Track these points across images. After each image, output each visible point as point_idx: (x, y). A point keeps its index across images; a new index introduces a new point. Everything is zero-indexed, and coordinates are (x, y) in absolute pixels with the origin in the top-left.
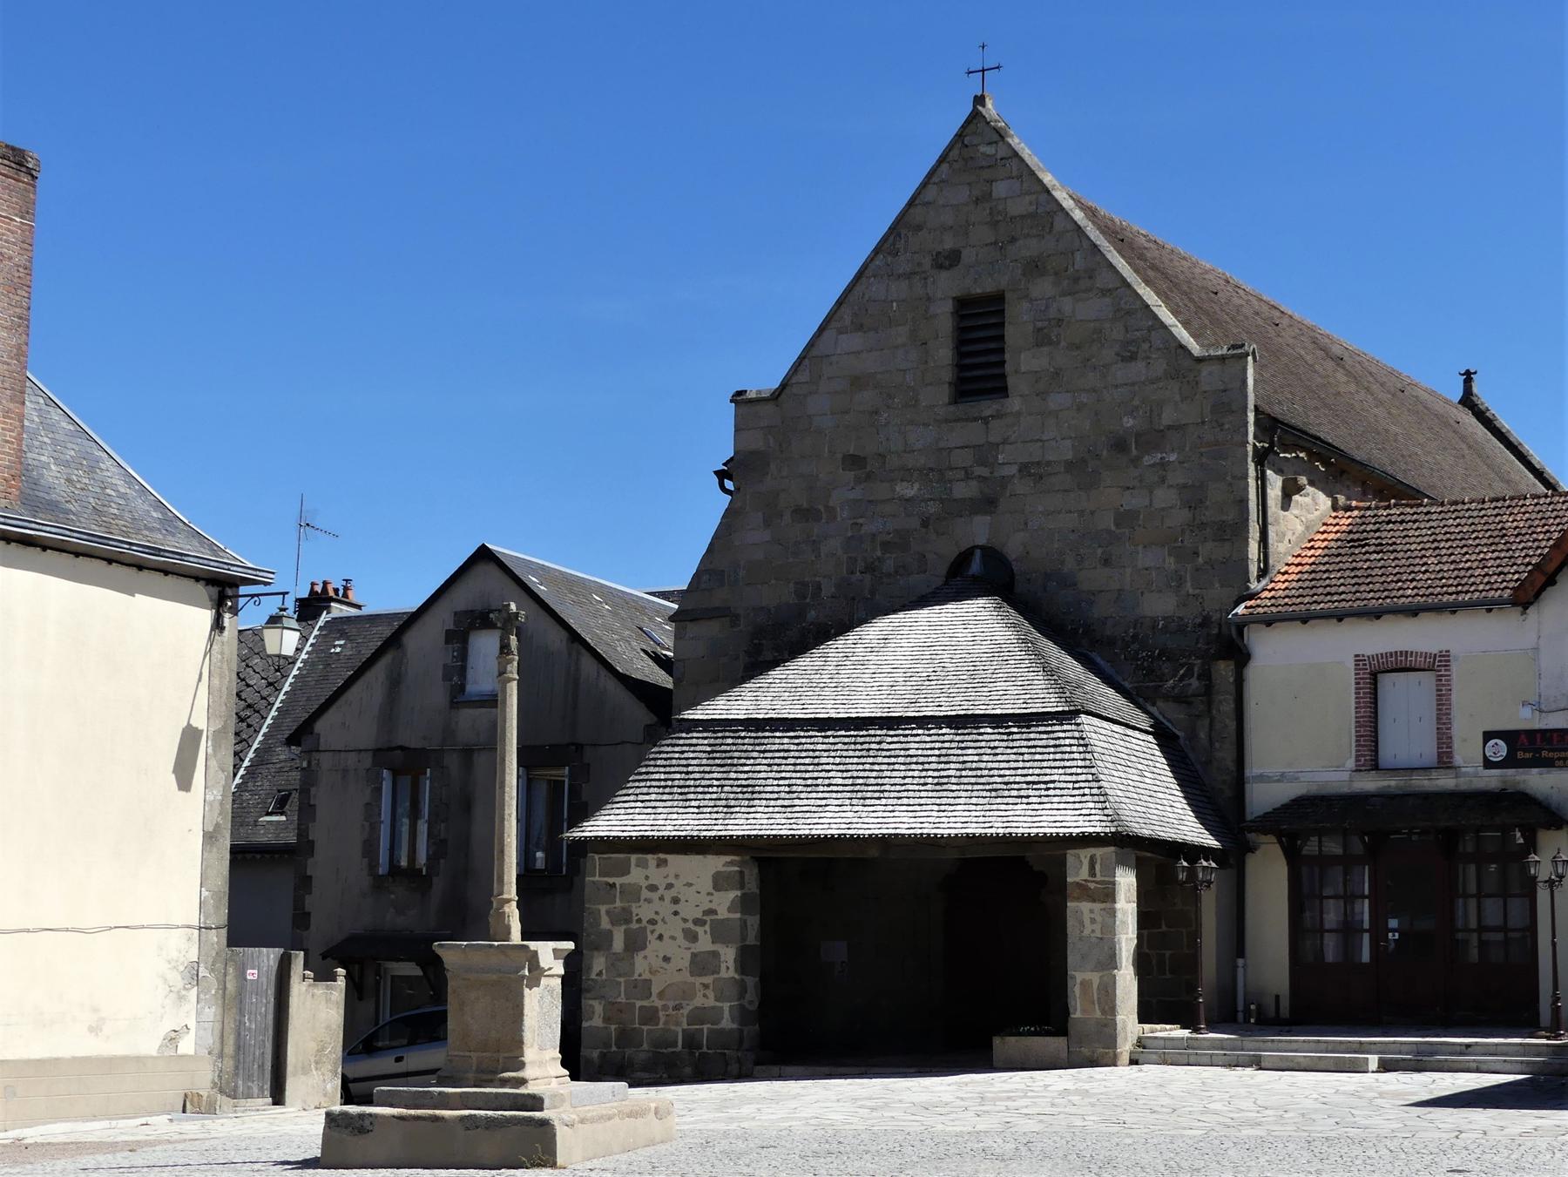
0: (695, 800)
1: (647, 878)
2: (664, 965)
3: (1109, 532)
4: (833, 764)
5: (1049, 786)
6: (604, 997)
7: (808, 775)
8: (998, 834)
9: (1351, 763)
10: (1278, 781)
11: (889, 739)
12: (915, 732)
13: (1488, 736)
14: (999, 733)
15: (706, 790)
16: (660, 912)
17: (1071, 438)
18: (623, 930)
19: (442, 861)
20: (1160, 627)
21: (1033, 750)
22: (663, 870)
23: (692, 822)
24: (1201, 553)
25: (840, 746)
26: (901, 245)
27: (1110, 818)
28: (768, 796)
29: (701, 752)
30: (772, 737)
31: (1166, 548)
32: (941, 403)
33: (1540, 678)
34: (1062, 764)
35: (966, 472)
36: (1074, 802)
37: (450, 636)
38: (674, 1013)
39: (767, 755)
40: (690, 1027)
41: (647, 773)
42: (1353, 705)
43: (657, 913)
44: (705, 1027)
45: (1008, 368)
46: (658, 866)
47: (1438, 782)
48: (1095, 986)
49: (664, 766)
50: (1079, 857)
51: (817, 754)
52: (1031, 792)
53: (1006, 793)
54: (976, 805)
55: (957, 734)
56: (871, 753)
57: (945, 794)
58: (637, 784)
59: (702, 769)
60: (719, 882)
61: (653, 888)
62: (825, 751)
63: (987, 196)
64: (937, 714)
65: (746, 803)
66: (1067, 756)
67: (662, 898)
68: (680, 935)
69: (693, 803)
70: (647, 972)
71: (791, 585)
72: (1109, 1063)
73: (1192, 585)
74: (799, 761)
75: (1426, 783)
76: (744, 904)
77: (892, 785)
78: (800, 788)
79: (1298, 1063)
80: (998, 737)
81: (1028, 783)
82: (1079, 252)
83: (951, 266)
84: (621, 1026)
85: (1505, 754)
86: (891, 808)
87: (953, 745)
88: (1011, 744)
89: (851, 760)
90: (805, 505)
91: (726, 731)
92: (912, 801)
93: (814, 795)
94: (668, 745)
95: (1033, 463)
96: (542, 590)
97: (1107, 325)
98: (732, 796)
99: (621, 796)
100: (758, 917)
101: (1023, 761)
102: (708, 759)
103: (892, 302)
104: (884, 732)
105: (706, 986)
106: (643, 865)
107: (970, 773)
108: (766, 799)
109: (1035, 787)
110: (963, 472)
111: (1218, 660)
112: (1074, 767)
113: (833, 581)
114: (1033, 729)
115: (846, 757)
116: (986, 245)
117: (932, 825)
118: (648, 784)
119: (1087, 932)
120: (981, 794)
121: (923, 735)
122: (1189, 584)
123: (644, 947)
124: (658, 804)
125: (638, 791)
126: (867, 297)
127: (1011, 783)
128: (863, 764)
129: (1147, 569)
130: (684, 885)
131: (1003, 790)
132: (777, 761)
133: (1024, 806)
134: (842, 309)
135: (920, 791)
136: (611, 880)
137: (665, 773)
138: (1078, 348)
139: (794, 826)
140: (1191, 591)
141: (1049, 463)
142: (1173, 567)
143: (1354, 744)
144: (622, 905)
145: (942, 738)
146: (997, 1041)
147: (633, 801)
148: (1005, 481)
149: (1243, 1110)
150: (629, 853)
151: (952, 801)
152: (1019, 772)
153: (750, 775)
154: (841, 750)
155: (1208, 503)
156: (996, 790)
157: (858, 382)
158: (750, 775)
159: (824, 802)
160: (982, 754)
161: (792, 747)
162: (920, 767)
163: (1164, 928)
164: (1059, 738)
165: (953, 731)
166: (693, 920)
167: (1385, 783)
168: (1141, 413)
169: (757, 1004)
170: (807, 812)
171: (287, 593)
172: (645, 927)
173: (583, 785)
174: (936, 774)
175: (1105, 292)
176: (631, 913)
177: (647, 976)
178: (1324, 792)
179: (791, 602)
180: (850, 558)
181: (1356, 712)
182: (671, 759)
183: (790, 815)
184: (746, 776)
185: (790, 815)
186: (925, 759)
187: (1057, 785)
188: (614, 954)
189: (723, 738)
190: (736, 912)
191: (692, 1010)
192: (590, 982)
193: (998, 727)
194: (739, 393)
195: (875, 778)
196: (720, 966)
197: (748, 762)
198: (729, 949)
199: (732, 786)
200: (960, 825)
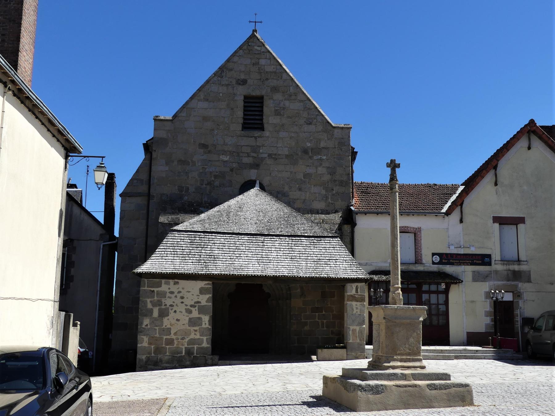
1: (169, 289)
2: (177, 322)
3: (301, 180)
6: (148, 335)
10: (365, 265)
13: (433, 254)
16: (175, 302)
17: (288, 147)
18: (158, 309)
22: (177, 286)
24: (334, 190)
26: (224, 74)
31: (322, 186)
33: (449, 238)
35: (248, 155)
38: (181, 341)
40: (188, 346)
43: (174, 302)
44: (195, 346)
45: (264, 121)
46: (174, 284)
47: (417, 268)
48: (357, 331)
50: (352, 287)
60: (202, 291)
61: (172, 293)
63: (258, 63)
67: (176, 297)
68: (184, 311)
71: (177, 187)
73: (331, 200)
75: (414, 268)
82: (292, 87)
83: (243, 84)
84: (156, 346)
85: (439, 260)
90: (183, 159)
95: (273, 154)
97: (301, 112)
103: (220, 93)
105: (196, 331)
106: (168, 284)
113: (194, 187)
116: (257, 79)
119: (354, 312)
122: (330, 200)
126: (210, 90)
129: (315, 193)
136: (152, 289)
138: (291, 118)
141: (279, 155)
142: (324, 193)
144: (158, 299)
148: (263, 159)
150: (161, 279)
155: (337, 174)
157: (205, 119)
163: (324, 313)
166: (190, 305)
168: (313, 142)
171: (104, 157)
172: (168, 308)
173: (73, 255)
175: (301, 101)
176: (162, 302)
177: (169, 326)
178: (381, 269)
179: (176, 193)
188: (154, 318)
190: (210, 303)
191: (189, 340)
194: (157, 116)
198: (206, 317)
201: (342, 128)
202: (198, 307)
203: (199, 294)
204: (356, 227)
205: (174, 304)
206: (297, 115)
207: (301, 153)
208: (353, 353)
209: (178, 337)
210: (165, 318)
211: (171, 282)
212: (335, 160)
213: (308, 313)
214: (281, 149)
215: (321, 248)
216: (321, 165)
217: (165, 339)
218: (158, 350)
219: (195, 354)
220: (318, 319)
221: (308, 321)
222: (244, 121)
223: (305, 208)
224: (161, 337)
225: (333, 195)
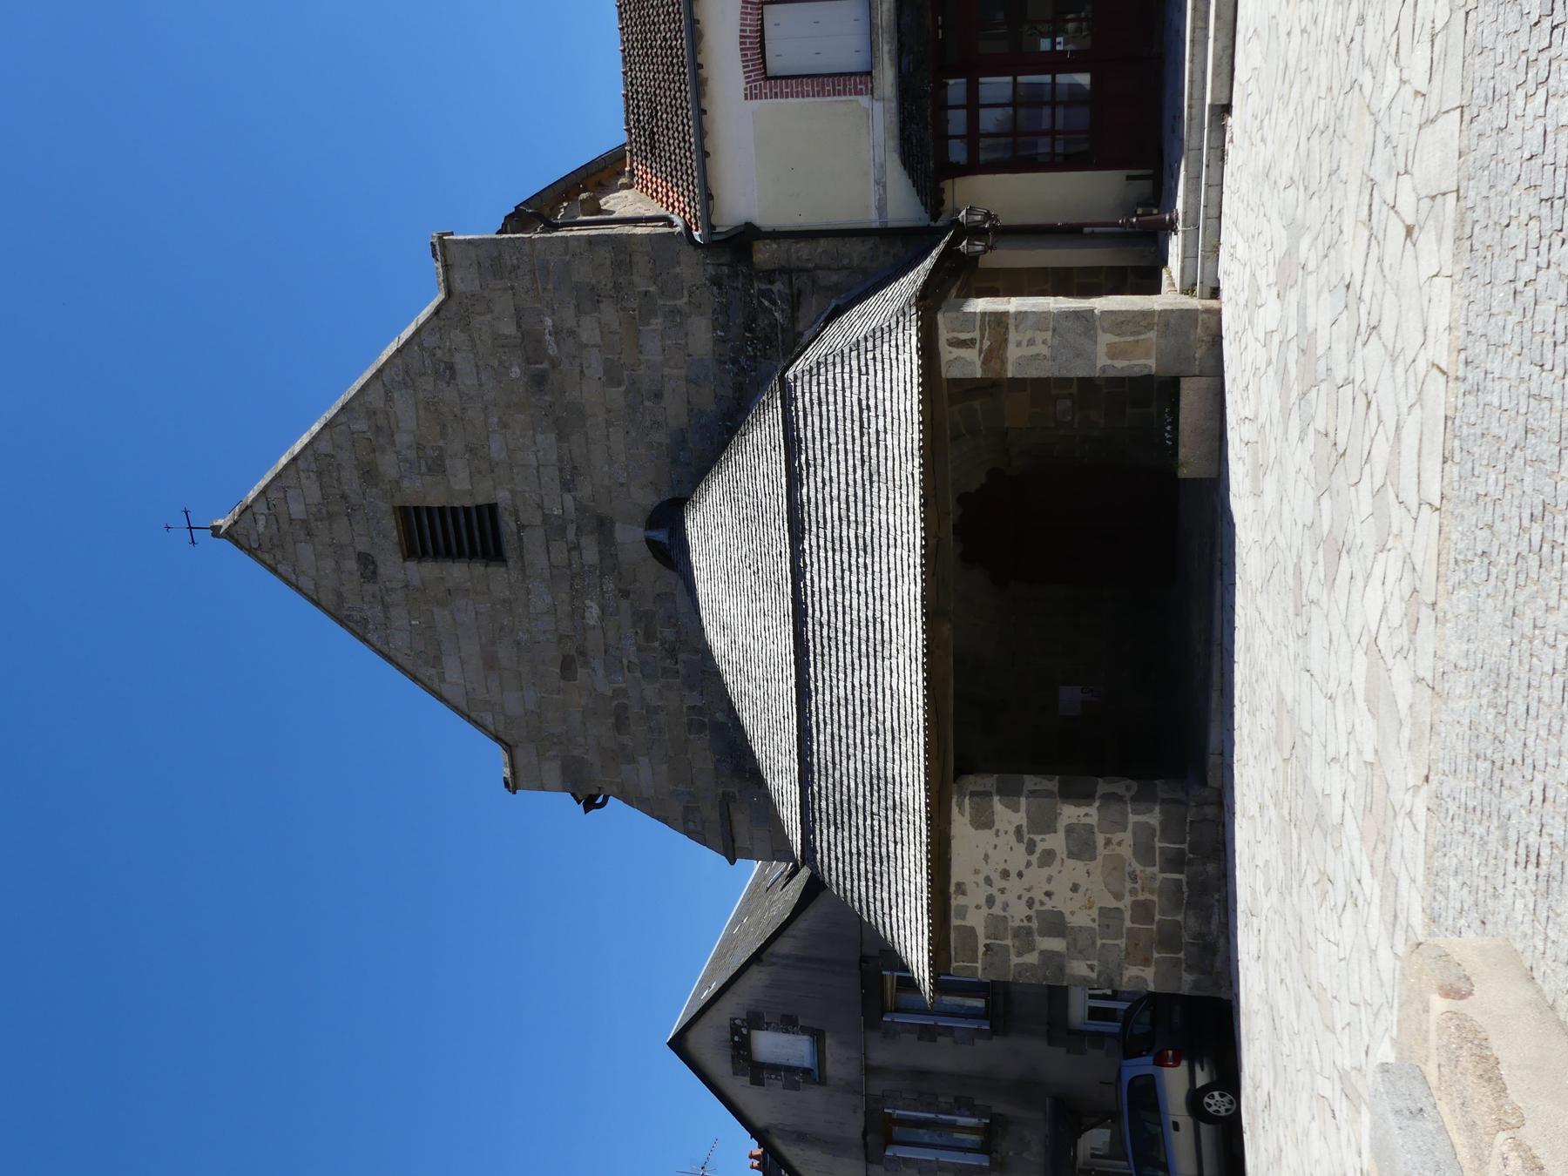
0: (888, 846)
1: (978, 907)
2: (1082, 890)
3: (627, 393)
4: (845, 681)
5: (864, 407)
6: (1119, 965)
7: (858, 712)
8: (920, 465)
9: (864, 100)
10: (884, 187)
11: (817, 613)
12: (809, 583)
14: (808, 477)
15: (876, 833)
17: (534, 436)
19: (976, 1102)
20: (722, 334)
21: (825, 432)
22: (970, 887)
23: (912, 852)
24: (644, 289)
25: (826, 674)
27: (901, 319)
28: (882, 760)
29: (836, 838)
30: (818, 754)
32: (506, 576)
34: (839, 393)
35: (573, 549)
36: (883, 370)
37: (757, 1081)
38: (1139, 881)
39: (837, 761)
41: (860, 901)
42: (800, 100)
43: (1020, 897)
44: (1158, 845)
45: (468, 503)
46: (964, 893)
48: (1115, 339)
49: (852, 880)
51: (835, 701)
52: (873, 430)
53: (874, 461)
54: (888, 499)
55: (810, 531)
56: (833, 635)
57: (876, 540)
58: (872, 913)
59: (854, 837)
60: (983, 821)
61: (990, 901)
62: (831, 691)
64: (788, 556)
65: (890, 786)
66: (831, 388)
67: (1002, 891)
68: (1046, 871)
69: (891, 849)
70: (1091, 912)
71: (692, 737)
72: (1215, 318)
74: (843, 722)
76: (1009, 793)
77: (867, 608)
78: (873, 721)
79: (1223, 51)
80: (812, 479)
81: (862, 435)
83: (373, 562)
86: (893, 608)
87: (822, 534)
88: (819, 461)
89: (841, 659)
90: (613, 720)
91: (813, 808)
92: (885, 582)
93: (880, 704)
94: (830, 875)
96: (714, 986)
97: (421, 395)
98: (883, 803)
99: (885, 932)
100: (1025, 776)
101: (837, 443)
102: (843, 830)
103: (411, 625)
104: (809, 620)
105: (1108, 842)
107: (852, 510)
108: (886, 761)
109: (866, 425)
110: (573, 553)
111: (752, 262)
112: (843, 377)
114: (802, 435)
115: (838, 666)
117: (912, 554)
118: (871, 900)
119: (1044, 350)
120: (875, 495)
121: (811, 572)
123: (1061, 914)
124: (893, 890)
125: (879, 912)
126: (408, 652)
127: (862, 456)
128: (845, 644)
130: (987, 863)
131: (870, 466)
132: (844, 749)
133: (889, 436)
134: (421, 676)
135: (873, 572)
136: (981, 949)
137: (859, 880)
138: (444, 426)
139: (915, 727)
140: (685, 300)
141: (560, 459)
142: (660, 320)
143: (843, 98)
144: (1010, 937)
145: (815, 549)
146: (1184, 473)
147: (891, 918)
148: (581, 508)
149: (1291, 87)
150: (949, 927)
151: (884, 531)
152: (849, 447)
153: (859, 780)
154: (830, 671)
155: (594, 281)
156: (871, 475)
157: (490, 662)
158: (859, 780)
159: (888, 692)
160: (831, 497)
161: (829, 730)
162: (847, 573)
164: (811, 400)
165: (807, 536)
167: (886, 57)
169: (1129, 782)
170: (899, 712)
172: (1038, 912)
174: (854, 554)
175: (388, 398)
176: (1020, 927)
177: (1095, 913)
180: (662, 675)
181: (808, 96)
182: (844, 872)
183: (903, 734)
184: (861, 786)
185: (903, 734)
186: (838, 568)
187: (863, 396)
188: (1068, 949)
189: (820, 812)
190: (1019, 801)
192: (1101, 980)
193: (801, 480)
194: (507, 784)
195: (860, 629)
196: (1084, 825)
197: (845, 783)
199: (872, 803)
200: (911, 516)
201: (447, 267)
202: (1034, 834)
203: (994, 829)
204: (758, 222)
205: (1026, 896)
206: (432, 408)
207: (546, 394)
208: (1197, 356)
209: (1127, 890)
210: (1067, 920)
211: (956, 901)
212: (550, 286)
214: (541, 453)
215: (825, 445)
216: (572, 333)
217: (1133, 923)
218: (1168, 939)
219: (1185, 846)
223: (715, 379)
224: (1127, 934)
225: (663, 293)
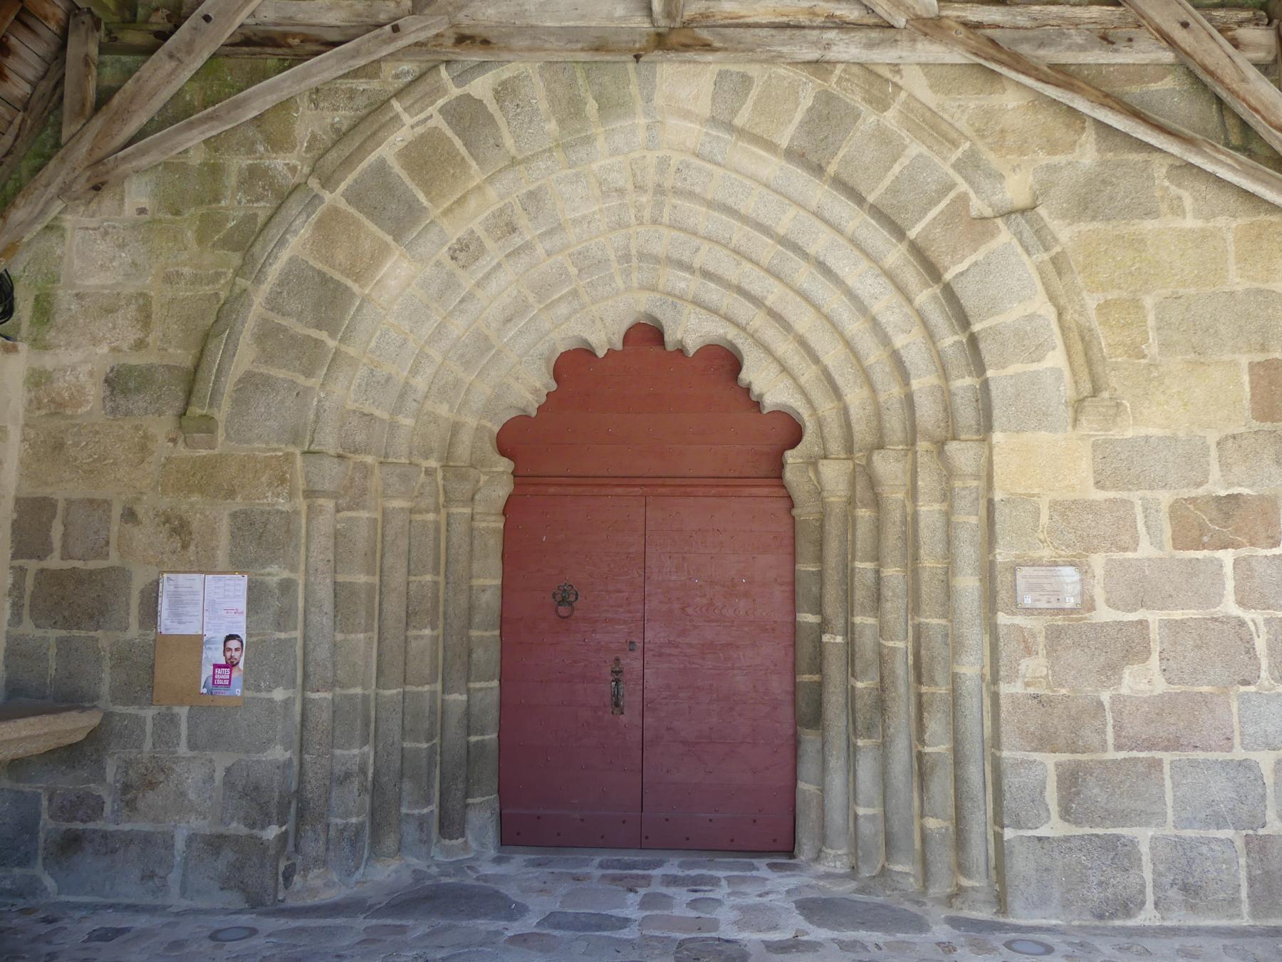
213: (1146, 550)
220: (1241, 603)
221: (1153, 617)
222: (222, 556)
